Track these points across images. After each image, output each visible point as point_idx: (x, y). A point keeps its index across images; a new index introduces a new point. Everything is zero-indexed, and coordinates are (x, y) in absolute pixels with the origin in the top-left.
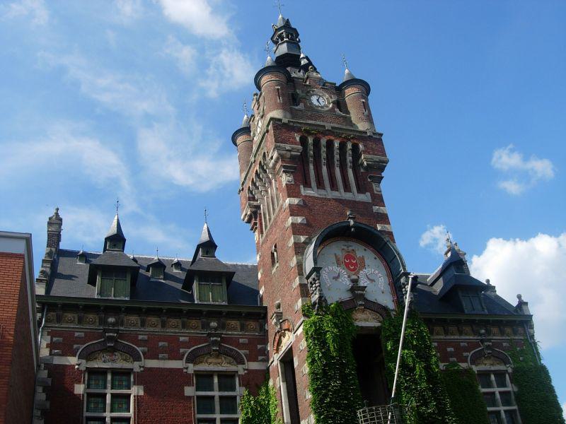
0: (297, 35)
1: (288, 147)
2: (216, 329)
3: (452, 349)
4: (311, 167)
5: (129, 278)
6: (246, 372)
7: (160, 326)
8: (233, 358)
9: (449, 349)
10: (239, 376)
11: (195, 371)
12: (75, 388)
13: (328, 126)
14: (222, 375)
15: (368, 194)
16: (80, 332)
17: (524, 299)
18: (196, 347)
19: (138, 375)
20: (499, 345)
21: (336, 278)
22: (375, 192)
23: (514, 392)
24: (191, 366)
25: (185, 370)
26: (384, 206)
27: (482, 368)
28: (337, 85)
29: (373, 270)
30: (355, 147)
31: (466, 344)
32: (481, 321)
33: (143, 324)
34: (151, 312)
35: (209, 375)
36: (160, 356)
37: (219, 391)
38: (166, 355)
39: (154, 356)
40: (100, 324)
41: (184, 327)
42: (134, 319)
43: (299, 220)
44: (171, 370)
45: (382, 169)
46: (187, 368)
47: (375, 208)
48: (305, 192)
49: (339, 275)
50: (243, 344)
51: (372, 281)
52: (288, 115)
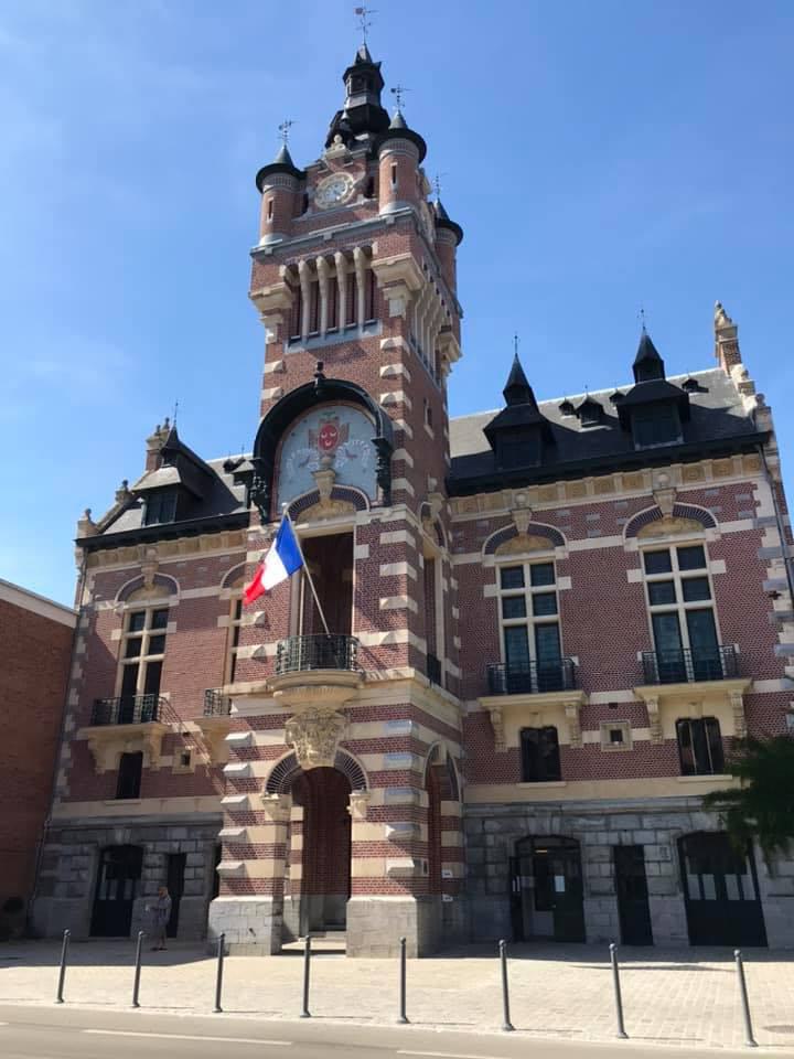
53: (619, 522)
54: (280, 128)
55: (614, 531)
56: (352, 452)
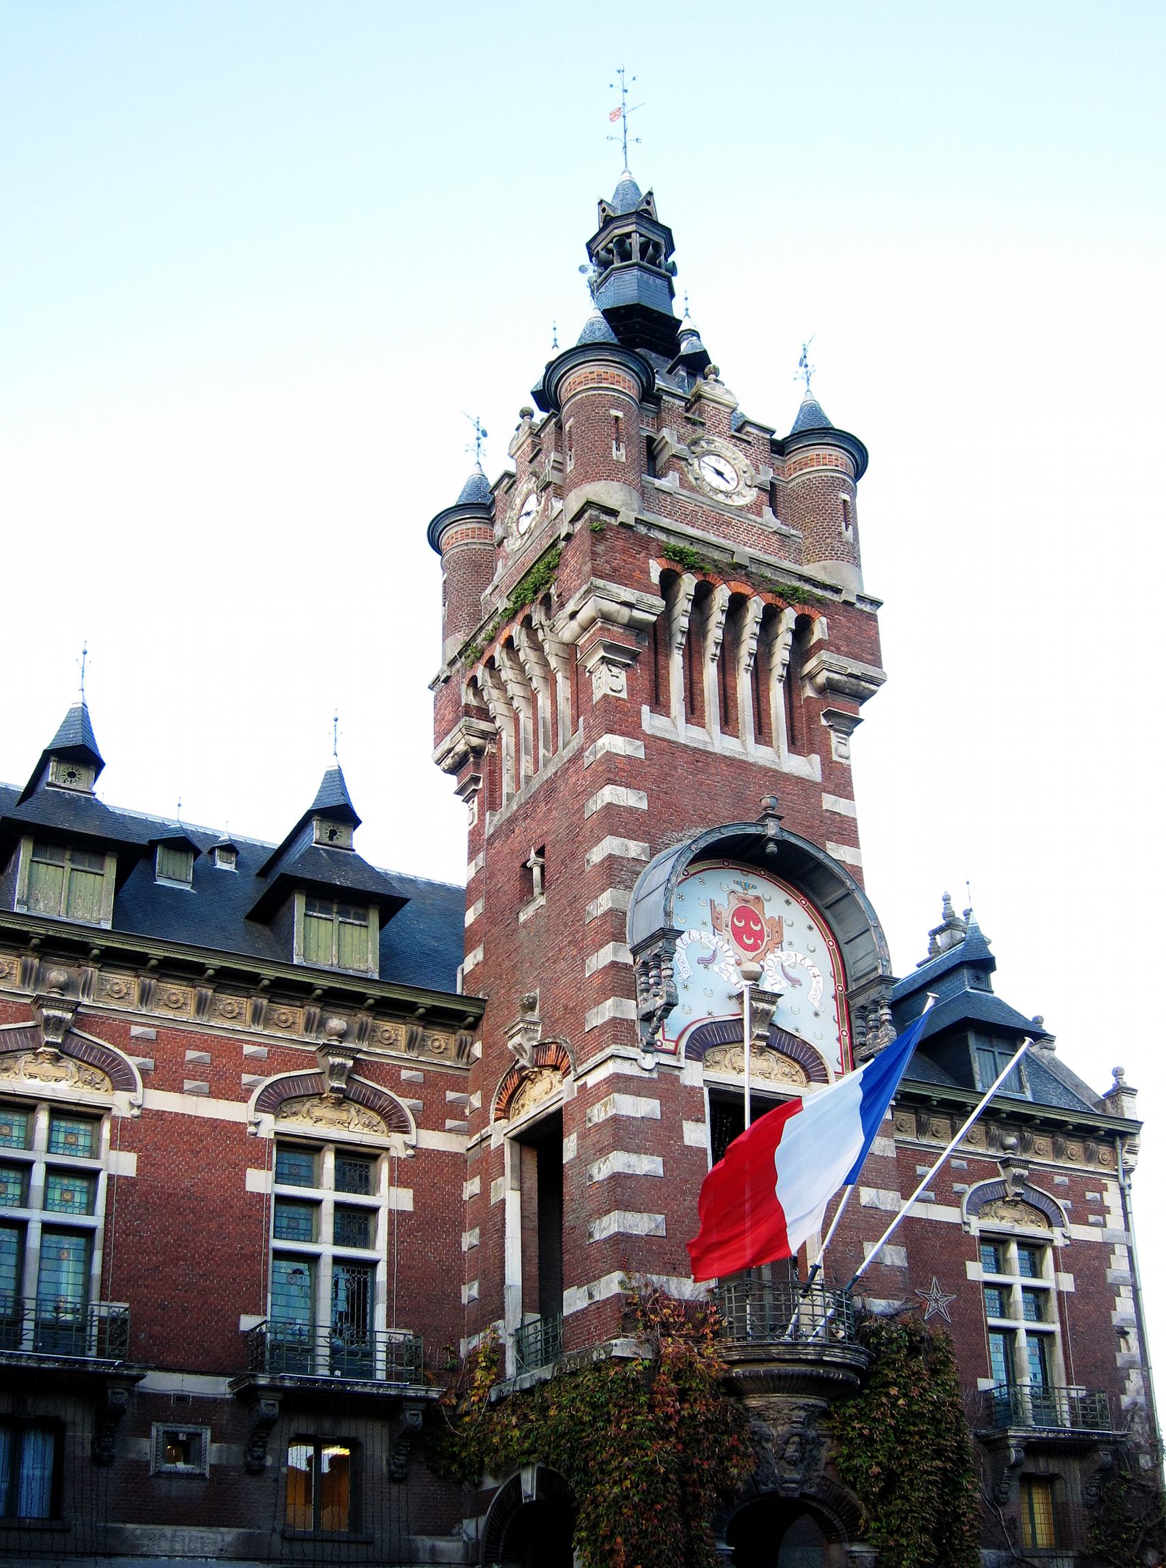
0: (671, 248)
1: (628, 594)
2: (342, 1036)
6: (411, 1152)
7: (248, 1017)
8: (379, 1113)
9: (191, 1055)
10: (114, 1120)
12: (405, 1190)
13: (745, 551)
15: (816, 758)
17: (1129, 1081)
18: (982, 1183)
20: (1043, 1178)
21: (706, 962)
22: (835, 758)
23: (1060, 1293)
24: (973, 1220)
25: (251, 1129)
26: (850, 796)
27: (993, 1224)
28: (779, 436)
29: (800, 956)
30: (803, 627)
31: (964, 1163)
32: (1013, 1116)
33: (146, 996)
34: (170, 969)
35: (312, 1147)
37: (337, 1189)
38: (205, 1086)
40: (23, 981)
41: (256, 1016)
42: (122, 980)
44: (214, 1124)
45: (862, 697)
46: (257, 1124)
47: (830, 802)
48: (650, 722)
50: (410, 1083)
51: (795, 982)
52: (636, 503)
53: (958, 1187)
55: (953, 1200)
56: (792, 973)
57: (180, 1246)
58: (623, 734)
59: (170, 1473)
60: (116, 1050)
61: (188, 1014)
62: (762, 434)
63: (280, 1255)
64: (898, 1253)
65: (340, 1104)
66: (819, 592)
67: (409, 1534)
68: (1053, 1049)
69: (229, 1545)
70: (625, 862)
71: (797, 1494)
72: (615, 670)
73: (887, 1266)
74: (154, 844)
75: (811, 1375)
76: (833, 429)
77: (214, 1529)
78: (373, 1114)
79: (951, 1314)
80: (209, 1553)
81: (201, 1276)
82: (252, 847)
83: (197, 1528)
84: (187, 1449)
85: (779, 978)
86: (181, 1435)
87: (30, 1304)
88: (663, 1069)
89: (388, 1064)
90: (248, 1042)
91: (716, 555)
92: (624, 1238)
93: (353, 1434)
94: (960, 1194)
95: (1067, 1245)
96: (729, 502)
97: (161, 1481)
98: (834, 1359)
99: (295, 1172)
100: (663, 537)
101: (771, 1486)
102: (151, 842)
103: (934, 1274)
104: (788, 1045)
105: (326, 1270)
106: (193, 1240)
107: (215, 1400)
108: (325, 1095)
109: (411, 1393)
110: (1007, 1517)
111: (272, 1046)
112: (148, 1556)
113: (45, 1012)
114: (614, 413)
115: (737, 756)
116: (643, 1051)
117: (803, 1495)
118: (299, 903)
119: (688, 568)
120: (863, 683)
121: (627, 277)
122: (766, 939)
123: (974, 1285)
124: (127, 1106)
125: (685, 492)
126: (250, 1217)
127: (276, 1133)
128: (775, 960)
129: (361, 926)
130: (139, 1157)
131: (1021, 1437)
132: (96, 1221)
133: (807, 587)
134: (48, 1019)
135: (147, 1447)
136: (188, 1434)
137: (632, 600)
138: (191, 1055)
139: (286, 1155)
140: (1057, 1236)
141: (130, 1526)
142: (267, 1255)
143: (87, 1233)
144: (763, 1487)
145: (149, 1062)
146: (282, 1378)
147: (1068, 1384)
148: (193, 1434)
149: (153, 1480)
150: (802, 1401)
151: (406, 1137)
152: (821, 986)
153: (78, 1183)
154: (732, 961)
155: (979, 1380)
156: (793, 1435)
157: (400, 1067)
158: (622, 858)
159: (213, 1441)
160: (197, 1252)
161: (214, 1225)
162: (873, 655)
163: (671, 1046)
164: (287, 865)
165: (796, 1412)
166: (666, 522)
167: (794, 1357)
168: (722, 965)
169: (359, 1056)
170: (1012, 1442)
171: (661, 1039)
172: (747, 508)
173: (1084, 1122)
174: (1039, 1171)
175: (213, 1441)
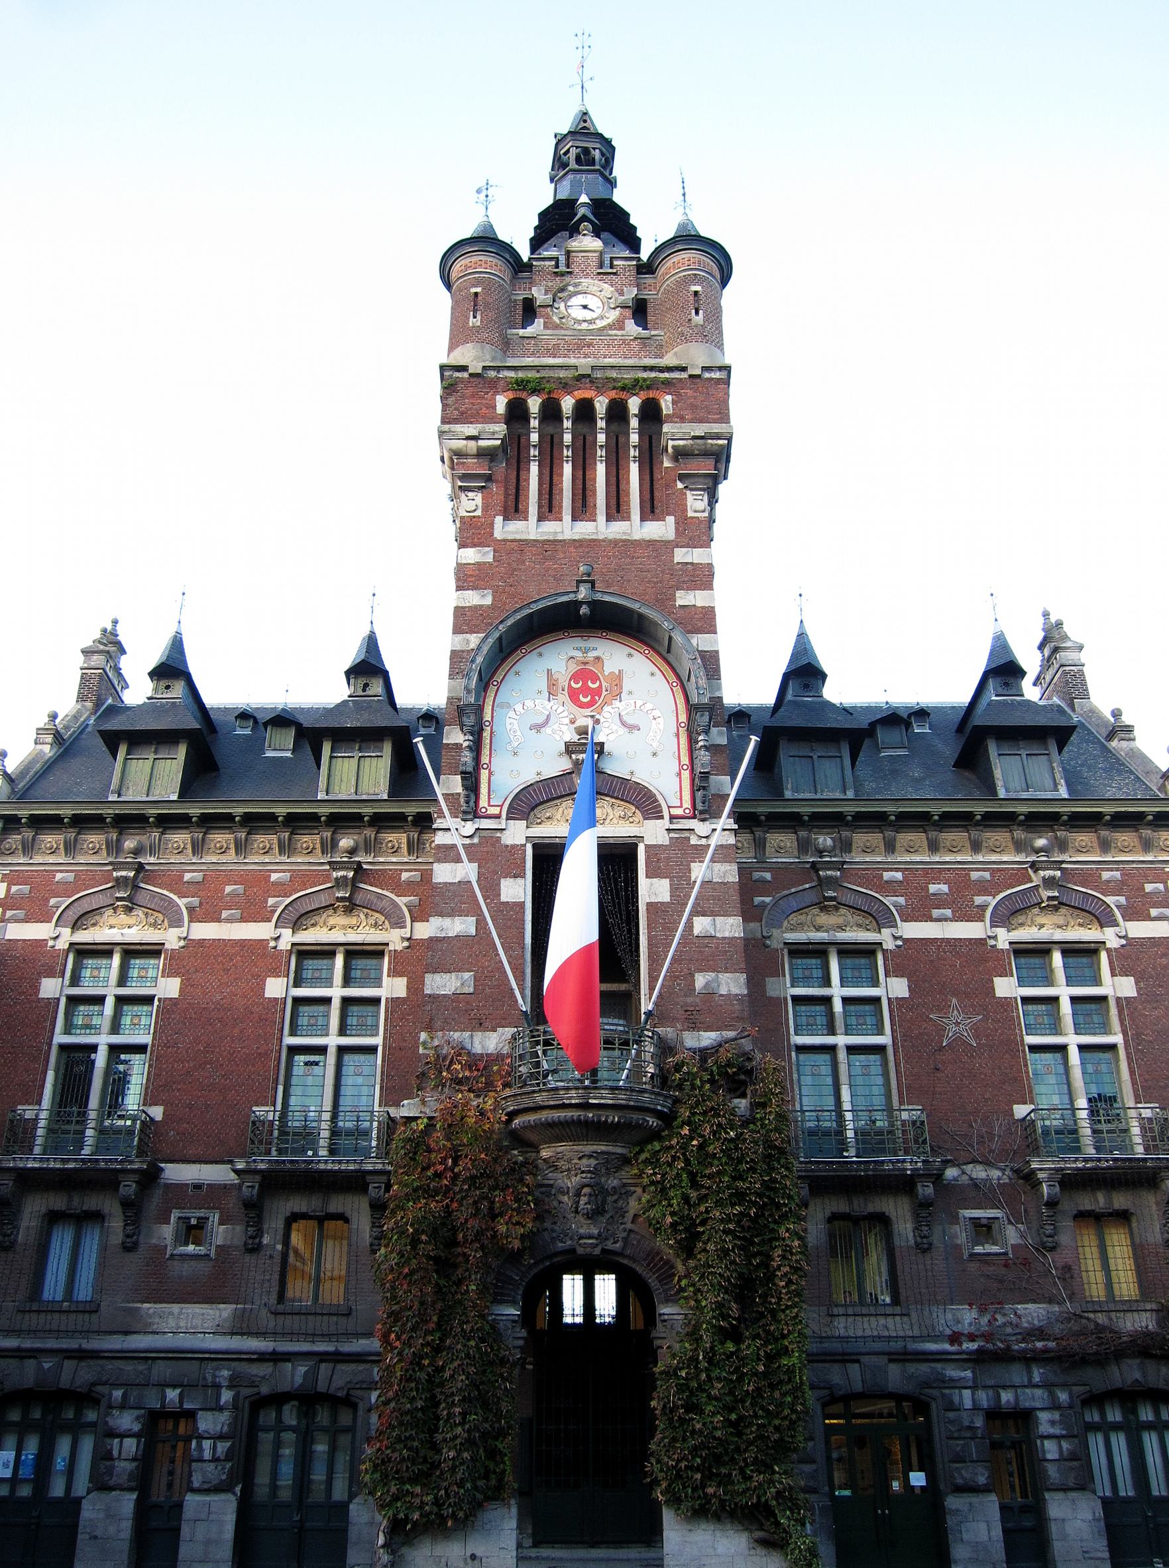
1: (471, 430)
3: (944, 888)
4: (568, 469)
5: (387, 748)
6: (1124, 942)
10: (1108, 951)
11: (293, 945)
14: (1072, 950)
16: (67, 871)
19: (174, 955)
20: (1089, 877)
21: (537, 728)
25: (992, 942)
34: (255, 822)
36: (225, 914)
38: (236, 913)
39: (212, 916)
43: (684, 598)
44: (243, 944)
47: (681, 555)
48: (503, 529)
49: (548, 717)
50: (409, 883)
53: (979, 900)
54: (479, 191)
55: (976, 915)
56: (630, 720)
57: (207, 1052)
58: (474, 545)
59: (181, 1255)
60: (172, 895)
61: (231, 856)
62: (630, 263)
63: (1034, 1048)
64: (736, 981)
65: (351, 911)
66: (666, 375)
67: (251, 1309)
68: (1134, 740)
69: (225, 1320)
70: (465, 654)
71: (597, 1251)
72: (471, 494)
73: (722, 995)
74: (873, 725)
75: (579, 1121)
76: (700, 236)
77: (214, 1306)
78: (377, 915)
79: (977, 1037)
80: (208, 1328)
81: (223, 1076)
82: (940, 710)
83: (201, 1306)
84: (193, 1231)
85: (614, 727)
86: (192, 1220)
87: (849, 1116)
88: (484, 833)
89: (390, 870)
90: (1103, 869)
91: (562, 374)
92: (431, 1000)
93: (340, 1210)
94: (983, 908)
95: (1122, 946)
96: (591, 327)
97: (176, 1263)
98: (602, 1101)
99: (1080, 974)
100: (512, 374)
101: (569, 1243)
102: (870, 724)
103: (954, 995)
104: (620, 789)
105: (1074, 1056)
106: (219, 1046)
107: (225, 1185)
108: (1043, 905)
109: (369, 1167)
110: (1059, 1265)
111: (294, 871)
112: (157, 1333)
113: (1042, 873)
114: (473, 290)
115: (587, 537)
116: (463, 820)
117: (604, 1251)
118: (993, 749)
119: (532, 392)
120: (710, 441)
121: (564, 183)
122: (604, 693)
123: (1007, 1003)
124: (176, 939)
125: (549, 332)
126: (266, 1020)
127: (1010, 943)
128: (612, 711)
129: (378, 756)
130: (182, 981)
131: (1050, 1169)
132: (885, 1039)
133: (653, 375)
134: (117, 879)
135: (167, 1232)
136: (199, 1218)
137: (475, 433)
138: (228, 889)
139: (1070, 960)
140: (1110, 937)
141: (146, 1305)
142: (1024, 1051)
143: (879, 1049)
144: (561, 1245)
145: (195, 901)
146: (255, 1161)
147: (1137, 1103)
148: (202, 1218)
149: (169, 1262)
150: (589, 1148)
151: (893, 930)
152: (661, 727)
153: (818, 1008)
154: (567, 721)
155: (1015, 1106)
156: (583, 1187)
157: (401, 870)
158: (463, 651)
159: (221, 1223)
160: (221, 1055)
161: (236, 1031)
162: (720, 413)
163: (496, 811)
164: (978, 720)
165: (585, 1161)
166: (528, 361)
167: (558, 1103)
168: (556, 727)
169: (1063, 866)
170: (1041, 1175)
171: (486, 806)
172: (611, 327)
173: (1123, 809)
174: (1082, 869)
175: (221, 1223)
